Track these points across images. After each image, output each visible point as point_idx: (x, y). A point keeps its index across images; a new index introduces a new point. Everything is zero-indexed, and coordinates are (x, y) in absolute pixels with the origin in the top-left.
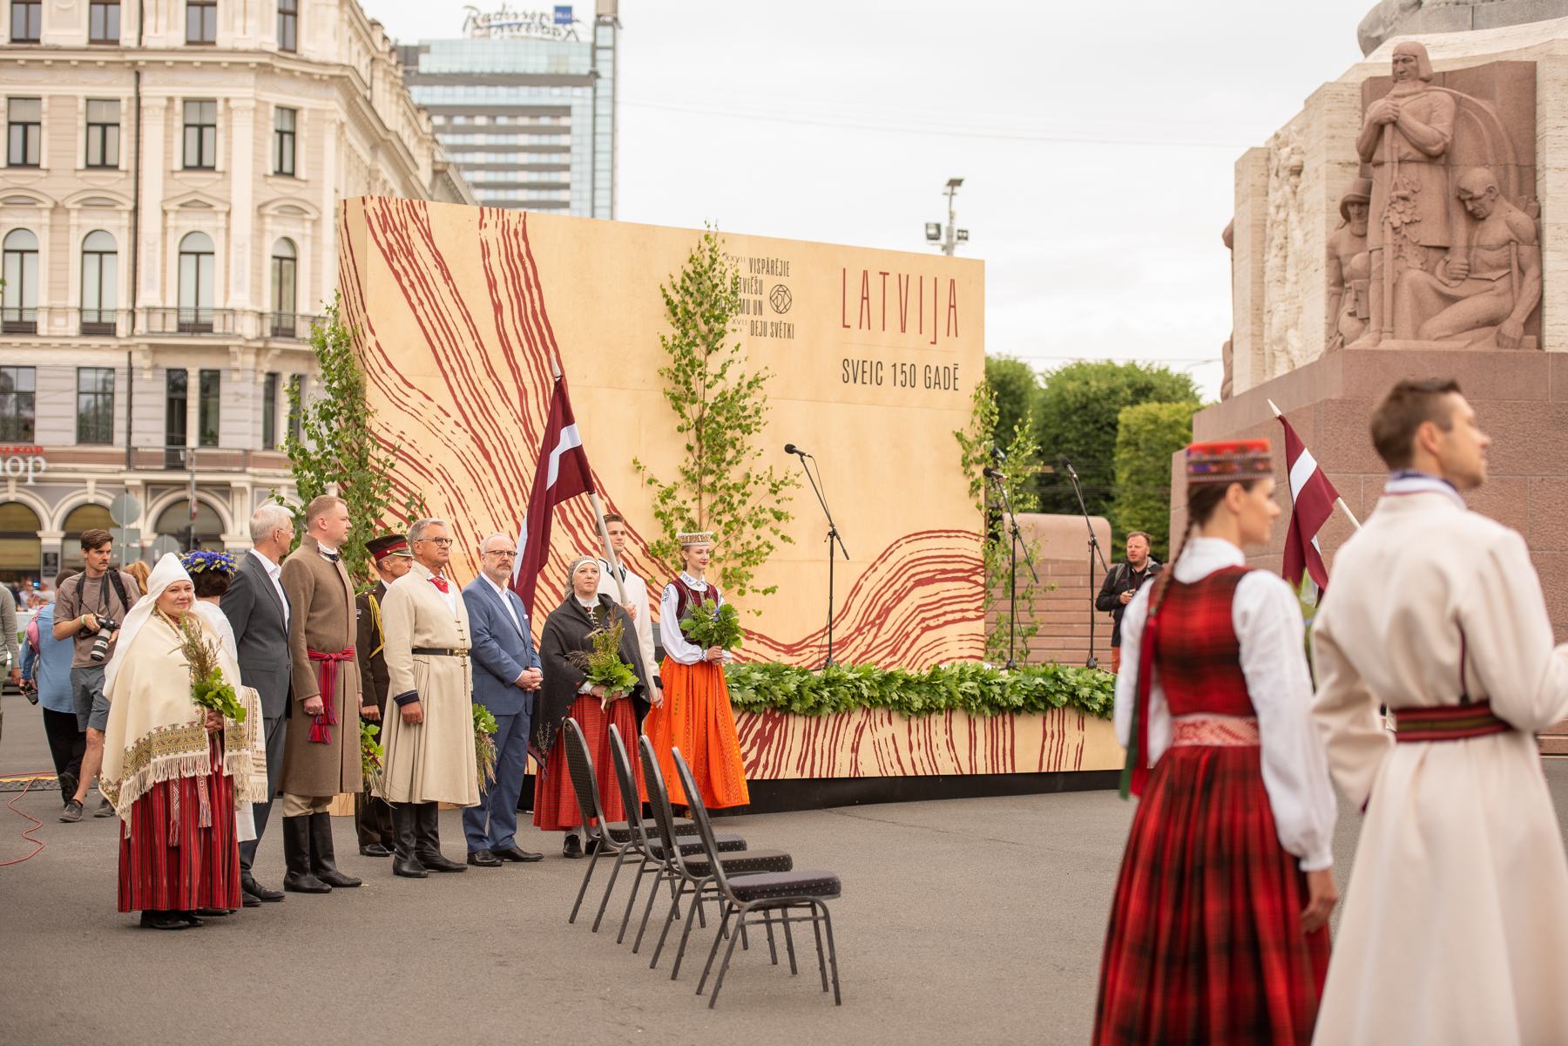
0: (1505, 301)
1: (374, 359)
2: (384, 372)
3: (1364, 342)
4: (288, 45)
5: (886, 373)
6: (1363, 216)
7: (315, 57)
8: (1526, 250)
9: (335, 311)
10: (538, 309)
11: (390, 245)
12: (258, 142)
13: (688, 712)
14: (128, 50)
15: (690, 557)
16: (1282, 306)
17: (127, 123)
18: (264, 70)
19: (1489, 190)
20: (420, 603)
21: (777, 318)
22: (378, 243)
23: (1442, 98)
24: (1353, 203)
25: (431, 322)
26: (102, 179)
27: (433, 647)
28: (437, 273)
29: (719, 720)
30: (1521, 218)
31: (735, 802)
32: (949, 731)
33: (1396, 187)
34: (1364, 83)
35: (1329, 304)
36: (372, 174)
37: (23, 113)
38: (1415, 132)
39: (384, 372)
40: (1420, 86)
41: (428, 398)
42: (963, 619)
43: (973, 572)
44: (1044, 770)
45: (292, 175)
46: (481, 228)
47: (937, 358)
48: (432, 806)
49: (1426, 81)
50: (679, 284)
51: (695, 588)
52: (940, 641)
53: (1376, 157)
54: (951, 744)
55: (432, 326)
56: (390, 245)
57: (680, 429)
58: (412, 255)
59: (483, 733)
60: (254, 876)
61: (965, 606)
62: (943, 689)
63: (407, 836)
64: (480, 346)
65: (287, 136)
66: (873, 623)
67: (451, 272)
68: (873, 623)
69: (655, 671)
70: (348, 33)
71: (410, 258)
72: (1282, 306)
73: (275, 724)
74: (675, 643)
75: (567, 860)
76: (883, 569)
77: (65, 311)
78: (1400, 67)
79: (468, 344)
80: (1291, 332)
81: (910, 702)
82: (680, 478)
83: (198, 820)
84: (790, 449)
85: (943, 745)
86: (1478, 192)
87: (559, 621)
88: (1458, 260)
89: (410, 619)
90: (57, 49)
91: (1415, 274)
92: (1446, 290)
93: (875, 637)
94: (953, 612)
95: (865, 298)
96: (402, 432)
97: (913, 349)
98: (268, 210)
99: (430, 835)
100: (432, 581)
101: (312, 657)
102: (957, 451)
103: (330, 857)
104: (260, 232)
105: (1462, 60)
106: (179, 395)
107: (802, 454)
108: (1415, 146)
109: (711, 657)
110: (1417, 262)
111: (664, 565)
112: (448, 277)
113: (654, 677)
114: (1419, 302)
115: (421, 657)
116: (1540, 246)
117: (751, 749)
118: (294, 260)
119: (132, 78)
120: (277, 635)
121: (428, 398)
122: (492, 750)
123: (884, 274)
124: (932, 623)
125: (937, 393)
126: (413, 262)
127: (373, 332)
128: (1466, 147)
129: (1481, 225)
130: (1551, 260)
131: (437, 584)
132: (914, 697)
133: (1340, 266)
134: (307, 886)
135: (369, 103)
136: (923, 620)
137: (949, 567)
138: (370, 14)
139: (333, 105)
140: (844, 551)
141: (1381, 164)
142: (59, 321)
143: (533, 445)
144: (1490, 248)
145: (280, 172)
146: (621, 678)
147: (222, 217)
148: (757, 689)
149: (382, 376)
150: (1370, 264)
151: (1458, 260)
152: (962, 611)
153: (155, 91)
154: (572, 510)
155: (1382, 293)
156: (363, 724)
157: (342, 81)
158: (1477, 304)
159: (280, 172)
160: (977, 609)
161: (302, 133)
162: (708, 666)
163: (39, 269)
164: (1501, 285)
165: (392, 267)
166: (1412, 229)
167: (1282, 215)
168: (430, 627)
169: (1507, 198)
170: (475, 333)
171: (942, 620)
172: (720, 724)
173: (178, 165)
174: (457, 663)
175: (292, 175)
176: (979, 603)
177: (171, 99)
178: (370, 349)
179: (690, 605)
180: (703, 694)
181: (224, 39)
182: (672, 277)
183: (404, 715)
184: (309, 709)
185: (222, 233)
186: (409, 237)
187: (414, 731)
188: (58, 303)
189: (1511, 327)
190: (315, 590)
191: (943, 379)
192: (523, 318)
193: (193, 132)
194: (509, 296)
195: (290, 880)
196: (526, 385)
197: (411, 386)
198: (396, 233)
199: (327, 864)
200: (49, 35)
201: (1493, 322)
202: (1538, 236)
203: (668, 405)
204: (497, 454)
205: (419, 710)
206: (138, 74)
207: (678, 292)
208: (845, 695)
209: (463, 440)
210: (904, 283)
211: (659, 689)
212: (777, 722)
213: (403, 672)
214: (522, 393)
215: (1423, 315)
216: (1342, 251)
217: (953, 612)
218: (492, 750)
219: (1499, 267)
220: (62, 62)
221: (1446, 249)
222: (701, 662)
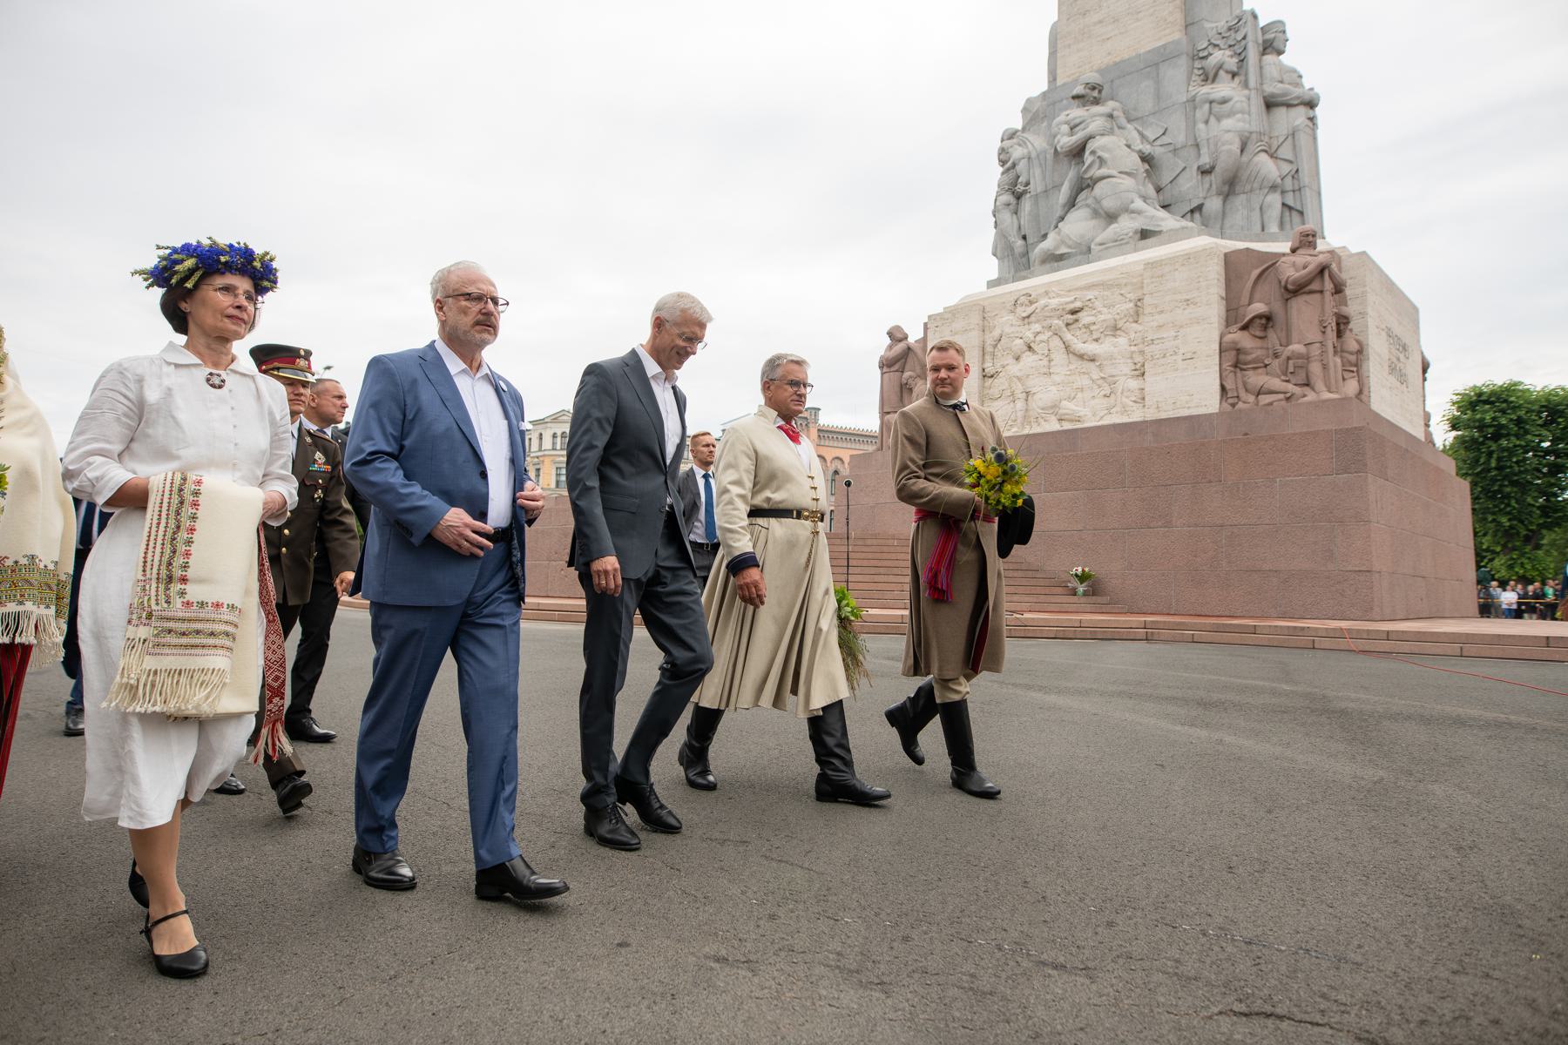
27: (774, 507)
38: (1304, 278)
50: (1283, 283)
131: (786, 432)
174: (806, 529)
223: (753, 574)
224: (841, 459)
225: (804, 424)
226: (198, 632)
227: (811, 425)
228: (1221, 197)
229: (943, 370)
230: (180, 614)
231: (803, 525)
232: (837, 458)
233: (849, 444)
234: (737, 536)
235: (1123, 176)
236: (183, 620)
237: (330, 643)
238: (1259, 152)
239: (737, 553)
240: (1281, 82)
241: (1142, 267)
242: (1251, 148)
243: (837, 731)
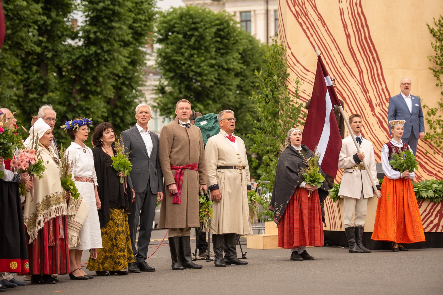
1: (290, 60)
2: (295, 65)
9: (276, 41)
10: (367, 36)
11: (297, 12)
13: (394, 200)
15: (394, 131)
20: (220, 147)
22: (292, 11)
25: (317, 44)
28: (319, 23)
29: (409, 204)
39: (295, 65)
46: (339, 3)
50: (438, 23)
51: (397, 145)
55: (318, 45)
56: (297, 12)
57: (437, 85)
58: (307, 16)
64: (340, 53)
67: (326, 22)
69: (377, 183)
71: (306, 17)
74: (388, 170)
79: (334, 52)
82: (438, 106)
83: (293, 244)
96: (305, 90)
100: (227, 137)
101: (172, 168)
109: (404, 176)
111: (431, 144)
112: (324, 24)
113: (377, 185)
117: (435, 218)
127: (290, 48)
143: (366, 94)
148: (435, 192)
149: (295, 67)
162: (404, 180)
170: (337, 47)
172: (410, 206)
178: (289, 56)
179: (394, 152)
180: (401, 192)
182: (434, 19)
184: (170, 190)
186: (306, 8)
190: (174, 139)
194: (354, 31)
196: (362, 69)
198: (300, 7)
203: (431, 75)
204: (349, 98)
205: (218, 193)
207: (437, 26)
211: (379, 191)
214: (361, 72)
222: (400, 178)
223: (216, 192)
226: (74, 227)
229: (185, 109)
231: (236, 171)
234: (212, 179)
239: (212, 184)
241: (105, 95)
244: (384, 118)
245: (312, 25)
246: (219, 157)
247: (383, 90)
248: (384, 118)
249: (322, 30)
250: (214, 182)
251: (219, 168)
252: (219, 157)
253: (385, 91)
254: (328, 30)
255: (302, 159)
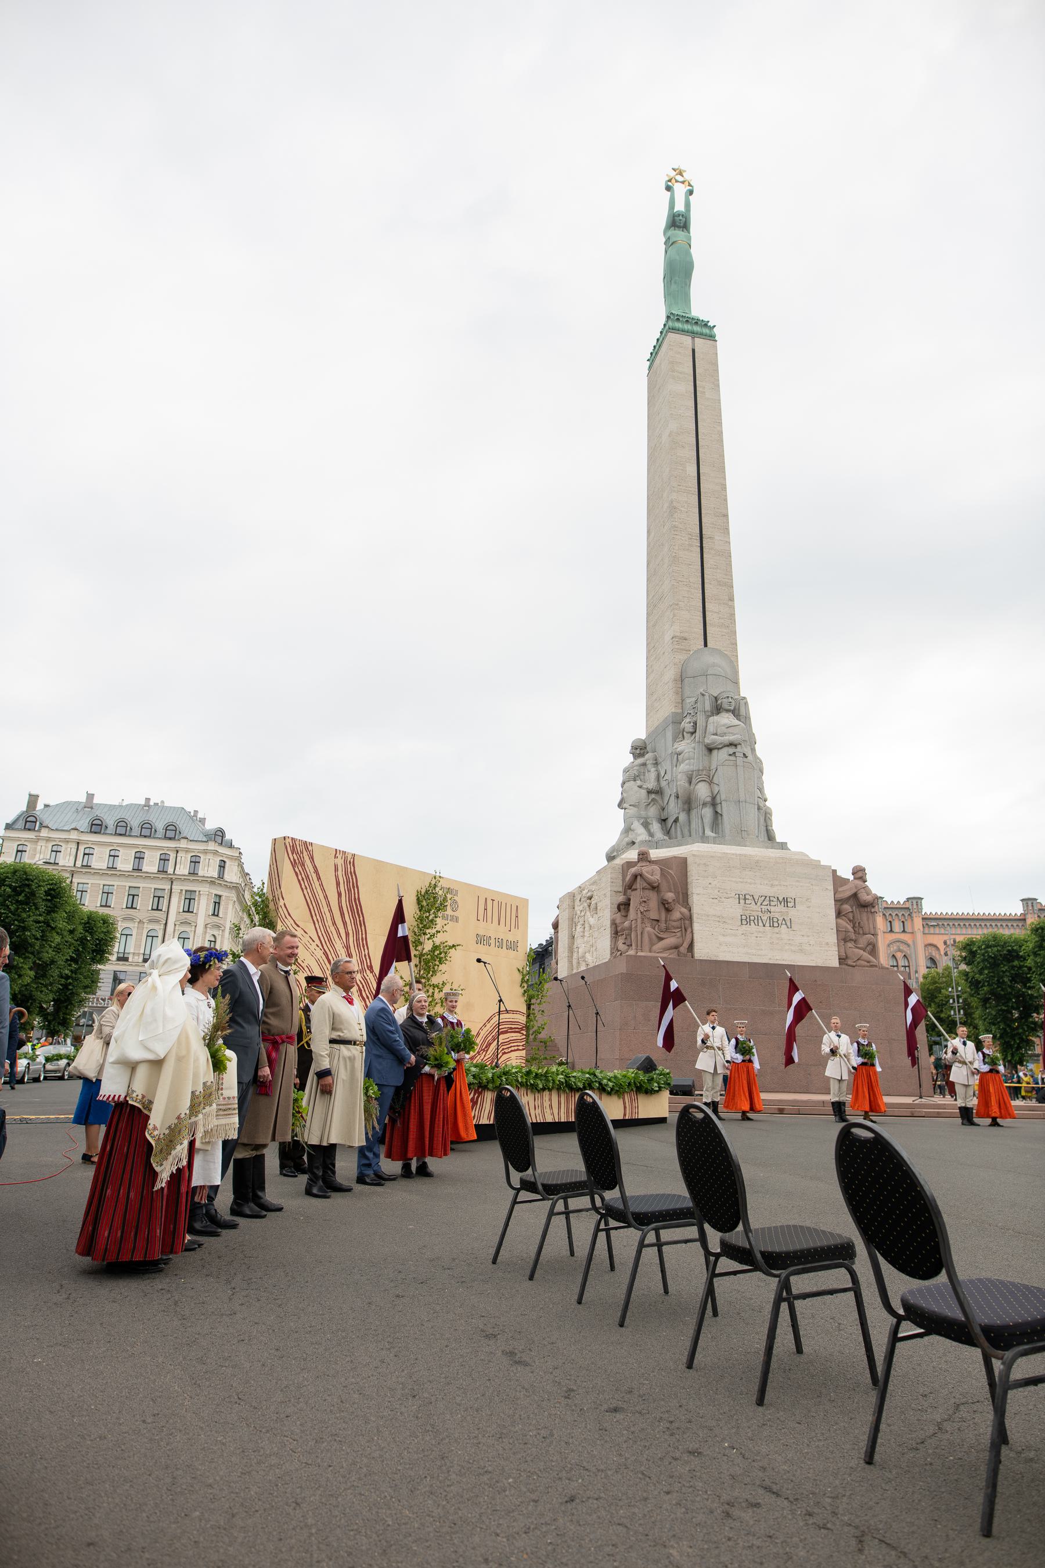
0: (680, 940)
1: (282, 911)
3: (631, 952)
4: (221, 876)
5: (492, 941)
6: (628, 910)
7: (229, 881)
8: (687, 922)
12: (208, 905)
14: (170, 874)
16: (583, 945)
17: (166, 897)
18: (212, 883)
19: (674, 900)
20: (336, 1011)
21: (453, 913)
23: (656, 867)
24: (622, 904)
26: (157, 914)
28: (314, 876)
30: (684, 910)
31: (472, 1138)
32: (550, 1100)
33: (642, 898)
34: (622, 866)
35: (611, 941)
36: (242, 919)
37: (133, 892)
40: (648, 864)
41: (306, 932)
42: (518, 1050)
43: (522, 1029)
44: (627, 1118)
45: (217, 916)
47: (511, 937)
48: (333, 1147)
49: (650, 862)
52: (509, 1059)
53: (633, 887)
54: (551, 1106)
59: (371, 1097)
60: (216, 1207)
61: (518, 1044)
62: (550, 1078)
63: (318, 1168)
64: (330, 911)
65: (217, 904)
66: (484, 1050)
68: (484, 1050)
70: (239, 875)
72: (583, 945)
73: (244, 1088)
75: (404, 1179)
76: (488, 1026)
77: (139, 954)
78: (641, 857)
79: (325, 909)
80: (587, 954)
81: (538, 1085)
84: (479, 961)
85: (548, 1107)
86: (670, 901)
87: (407, 1029)
88: (663, 925)
89: (330, 1021)
90: (147, 873)
91: (649, 929)
92: (659, 935)
93: (485, 1056)
94: (514, 1046)
95: (486, 909)
97: (501, 932)
98: (208, 926)
99: (330, 1166)
100: (344, 997)
102: (519, 977)
103: (263, 1189)
104: (205, 933)
105: (657, 858)
106: (679, 234)
107: (485, 963)
108: (649, 884)
110: (649, 925)
112: (319, 878)
114: (650, 940)
115: (335, 1046)
116: (691, 921)
118: (215, 942)
119: (170, 883)
120: (251, 1018)
121: (306, 932)
122: (376, 1109)
123: (493, 900)
124: (506, 1051)
125: (511, 951)
126: (304, 869)
128: (664, 887)
129: (670, 913)
130: (696, 926)
132: (539, 1082)
133: (616, 927)
134: (248, 1212)
135: (243, 896)
136: (503, 1049)
137: (513, 1026)
138: (246, 871)
139: (233, 895)
140: (694, 351)
141: (636, 889)
142: (136, 957)
144: (674, 921)
145: (214, 915)
146: (447, 1063)
147: (194, 927)
148: (474, 1076)
149: (286, 920)
150: (631, 925)
151: (663, 925)
152: (518, 1046)
153: (176, 888)
154: (365, 991)
155: (637, 935)
156: (296, 1090)
157: (236, 888)
158: (671, 941)
159: (214, 915)
160: (523, 1046)
161: (222, 903)
163: (132, 941)
164: (679, 934)
165: (294, 870)
166: (647, 913)
167: (583, 914)
168: (341, 1027)
169: (679, 903)
170: (328, 905)
171: (510, 1049)
173: (181, 910)
174: (357, 1050)
175: (217, 916)
176: (524, 1043)
177: (181, 890)
181: (201, 873)
183: (322, 1085)
185: (193, 932)
187: (327, 1097)
188: (137, 952)
189: (683, 949)
191: (513, 946)
192: (350, 901)
193: (187, 901)
195: (235, 1207)
197: (298, 926)
199: (260, 1194)
200: (145, 868)
201: (676, 947)
202: (691, 918)
206: (172, 882)
208: (512, 1080)
209: (319, 953)
210: (500, 904)
212: (480, 1093)
213: (323, 1055)
214: (347, 934)
215: (652, 944)
216: (618, 921)
217: (514, 1046)
218: (376, 1109)
219: (678, 928)
220: (149, 877)
221: (658, 921)
224: (935, 946)
225: (906, 915)
226: (230, 1109)
227: (914, 915)
228: (685, 812)
230: (223, 1103)
232: (931, 945)
233: (969, 930)
235: (631, 807)
236: (224, 1105)
237: (754, 732)
238: (699, 781)
240: (716, 734)
242: (694, 781)
243: (1005, 1354)
244: (363, 987)
245: (307, 877)
246: (334, 1026)
247: (365, 956)
248: (363, 987)
249: (316, 884)
250: (325, 1064)
251: (333, 1041)
252: (334, 1026)
253: (367, 957)
254: (321, 885)
255: (427, 1034)
